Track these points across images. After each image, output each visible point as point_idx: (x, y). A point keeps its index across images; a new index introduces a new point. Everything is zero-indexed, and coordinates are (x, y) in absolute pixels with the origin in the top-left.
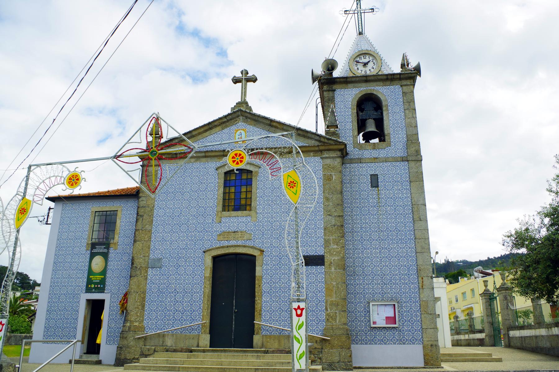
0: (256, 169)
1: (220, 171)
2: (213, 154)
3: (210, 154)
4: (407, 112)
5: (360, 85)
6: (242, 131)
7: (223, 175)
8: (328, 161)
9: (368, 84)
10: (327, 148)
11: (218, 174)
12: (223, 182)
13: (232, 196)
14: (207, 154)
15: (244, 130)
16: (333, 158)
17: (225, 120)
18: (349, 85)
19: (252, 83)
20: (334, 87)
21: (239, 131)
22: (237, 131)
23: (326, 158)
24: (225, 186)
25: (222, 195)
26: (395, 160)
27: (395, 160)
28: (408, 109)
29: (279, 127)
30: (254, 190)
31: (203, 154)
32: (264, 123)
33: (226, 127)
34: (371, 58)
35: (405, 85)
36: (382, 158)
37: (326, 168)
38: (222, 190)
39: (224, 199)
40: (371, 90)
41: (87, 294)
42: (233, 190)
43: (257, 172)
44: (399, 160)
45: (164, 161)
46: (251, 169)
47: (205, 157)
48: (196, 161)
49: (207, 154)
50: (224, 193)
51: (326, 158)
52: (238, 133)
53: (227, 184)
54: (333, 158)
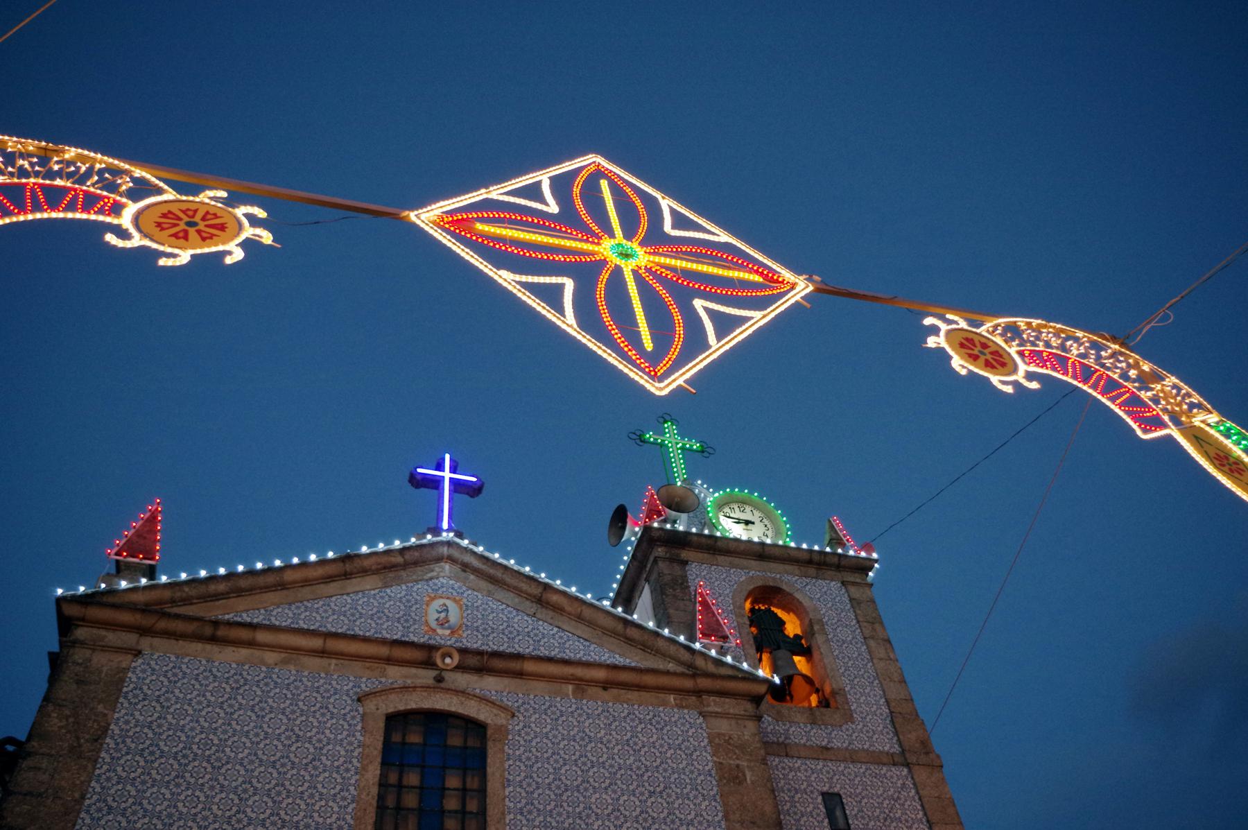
0: (501, 719)
1: (371, 705)
2: (354, 647)
3: (342, 646)
4: (872, 643)
5: (745, 562)
6: (448, 602)
7: (382, 724)
8: (724, 726)
9: (764, 564)
10: (719, 685)
11: (363, 716)
12: (380, 745)
13: (411, 800)
14: (332, 645)
15: (455, 600)
16: (736, 717)
17: (400, 559)
18: (721, 559)
19: (466, 497)
20: (684, 554)
21: (441, 601)
22: (433, 599)
23: (717, 715)
24: (385, 763)
25: (375, 790)
26: (876, 759)
27: (876, 759)
28: (872, 637)
29: (568, 608)
30: (493, 785)
31: (317, 643)
32: (518, 591)
33: (399, 581)
34: (757, 514)
35: (854, 584)
36: (838, 749)
37: (719, 744)
38: (374, 771)
39: (381, 808)
40: (774, 579)
41: (47, 659)
42: (413, 779)
43: (503, 731)
44: (885, 760)
45: (156, 641)
46: (482, 717)
47: (322, 653)
48: (285, 662)
49: (332, 645)
50: (383, 784)
51: (717, 715)
52: (437, 604)
53: (392, 756)
54: (736, 717)
